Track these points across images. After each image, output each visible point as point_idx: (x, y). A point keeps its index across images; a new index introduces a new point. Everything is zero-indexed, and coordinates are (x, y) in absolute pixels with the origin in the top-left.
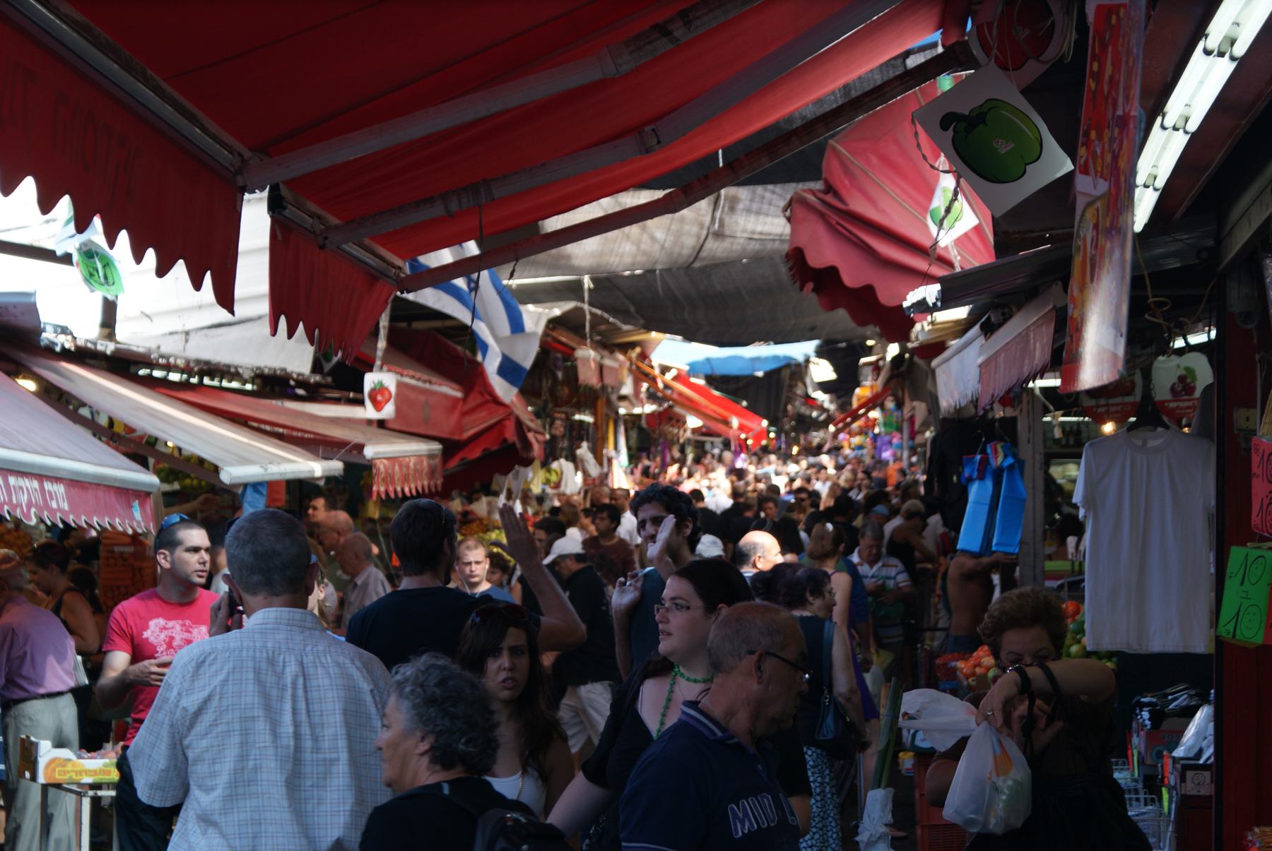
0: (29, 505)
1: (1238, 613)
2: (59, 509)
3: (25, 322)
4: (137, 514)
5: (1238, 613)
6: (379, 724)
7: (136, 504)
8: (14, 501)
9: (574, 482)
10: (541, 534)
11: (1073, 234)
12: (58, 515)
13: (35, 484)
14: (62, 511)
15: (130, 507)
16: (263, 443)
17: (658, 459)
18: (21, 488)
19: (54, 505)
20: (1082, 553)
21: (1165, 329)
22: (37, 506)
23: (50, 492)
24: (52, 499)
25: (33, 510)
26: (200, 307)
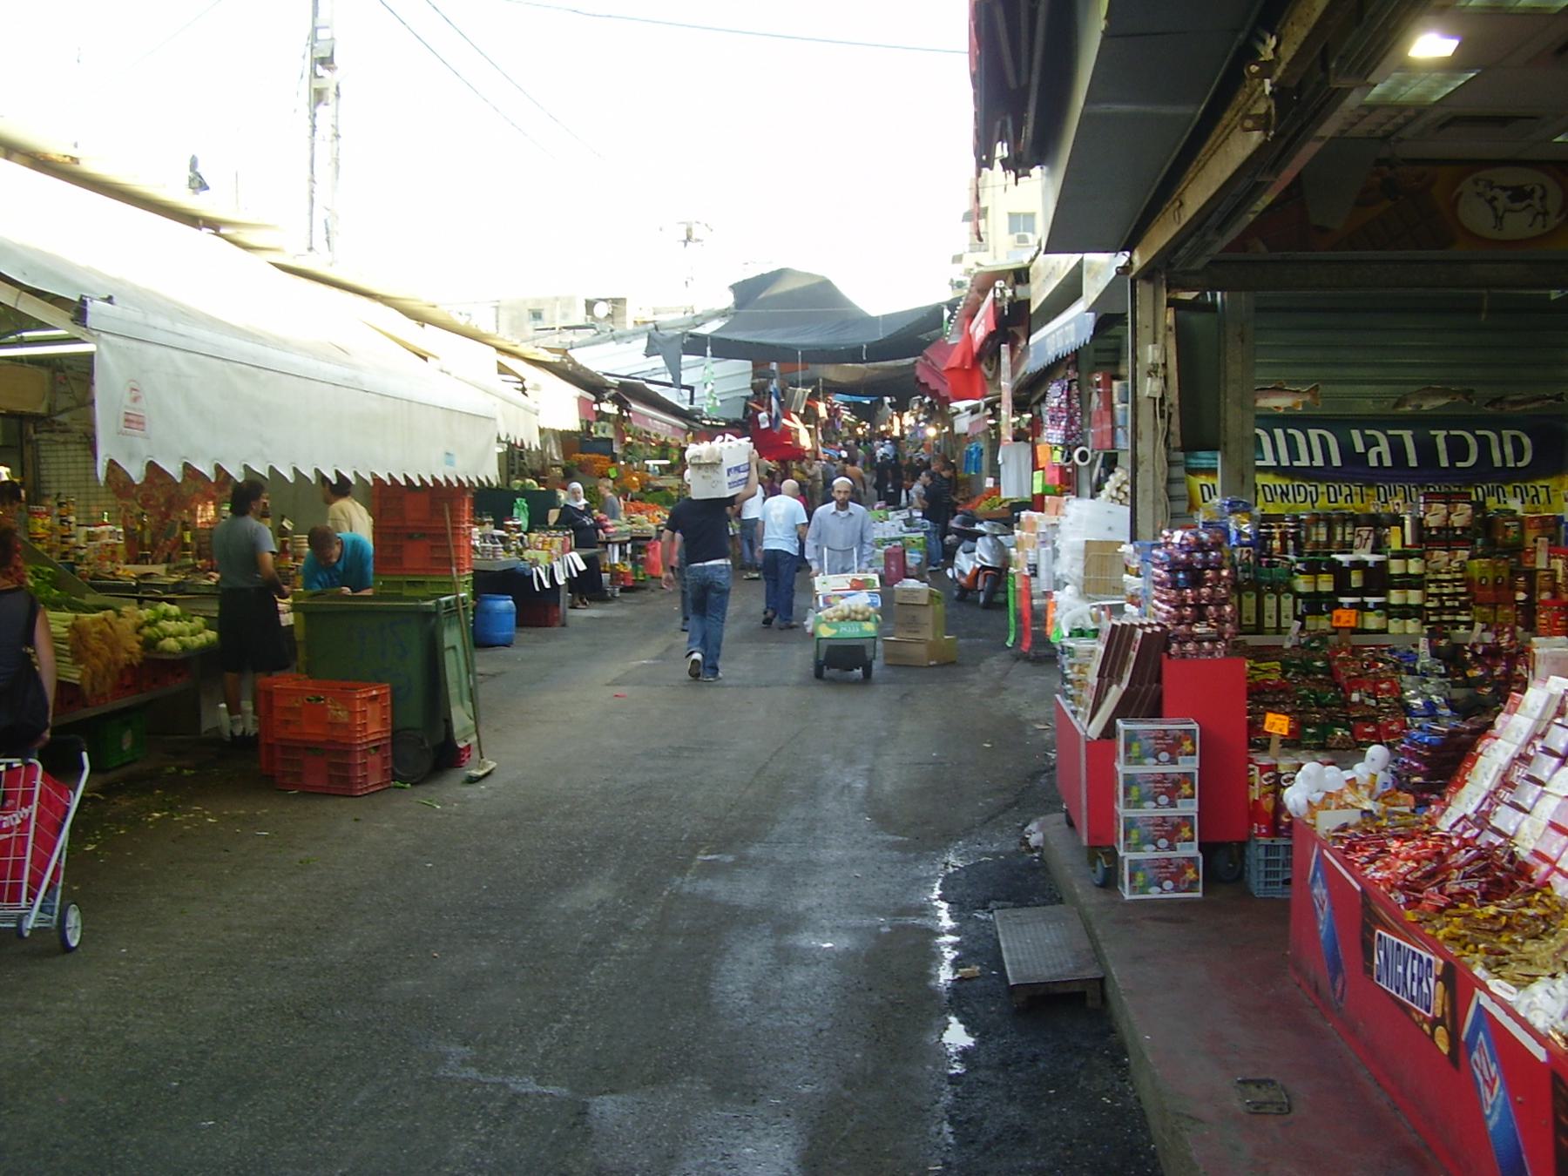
11: (808, 400)
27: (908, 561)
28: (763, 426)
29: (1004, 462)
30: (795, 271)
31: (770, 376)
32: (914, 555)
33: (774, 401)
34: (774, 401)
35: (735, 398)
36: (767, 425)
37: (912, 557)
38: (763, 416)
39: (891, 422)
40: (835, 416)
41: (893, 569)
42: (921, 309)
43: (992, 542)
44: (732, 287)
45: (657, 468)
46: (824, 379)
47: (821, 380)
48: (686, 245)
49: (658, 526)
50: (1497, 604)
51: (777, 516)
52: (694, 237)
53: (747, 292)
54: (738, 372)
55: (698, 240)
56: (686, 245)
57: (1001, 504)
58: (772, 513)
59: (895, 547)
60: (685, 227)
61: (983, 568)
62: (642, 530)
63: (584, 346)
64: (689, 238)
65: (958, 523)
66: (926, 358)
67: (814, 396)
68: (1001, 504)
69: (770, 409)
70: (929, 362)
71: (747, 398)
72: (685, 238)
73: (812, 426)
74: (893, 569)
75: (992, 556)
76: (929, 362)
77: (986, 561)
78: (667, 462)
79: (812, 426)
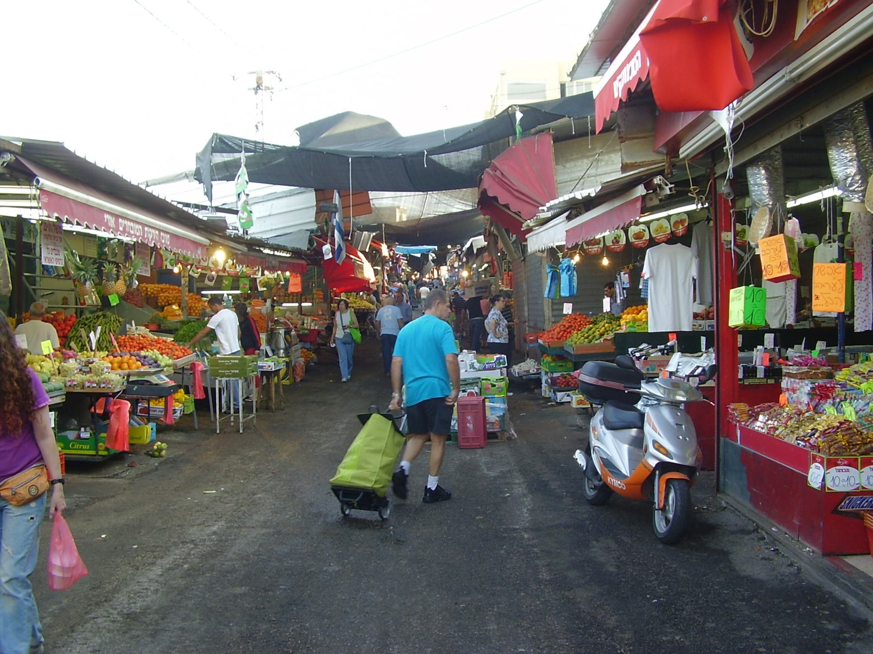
0: (152, 239)
1: (752, 314)
2: (165, 243)
3: (223, 224)
4: (199, 252)
5: (752, 314)
6: (849, 357)
7: (200, 248)
8: (146, 236)
9: (492, 627)
10: (771, 381)
11: (372, 241)
12: (164, 245)
13: (157, 232)
14: (166, 244)
15: (197, 249)
16: (177, 232)
17: (440, 529)
18: (150, 232)
19: (163, 241)
20: (378, 243)
21: (14, 556)
22: (155, 240)
23: (163, 237)
24: (163, 239)
25: (153, 242)
26: (272, 230)
27: (488, 413)
28: (326, 258)
29: (652, 276)
30: (354, 113)
31: (333, 211)
32: (498, 405)
33: (336, 234)
34: (336, 234)
35: (300, 231)
36: (330, 256)
37: (492, 408)
38: (327, 248)
39: (433, 273)
40: (397, 263)
41: (470, 426)
42: (476, 124)
43: (674, 416)
44: (297, 129)
45: (230, 297)
46: (385, 224)
47: (383, 225)
48: (256, 93)
49: (129, 376)
50: (180, 262)
51: (387, 316)
52: (264, 85)
53: (307, 132)
54: (303, 206)
55: (267, 88)
56: (256, 93)
57: (602, 335)
58: (385, 315)
59: (471, 394)
60: (255, 76)
61: (663, 467)
62: (98, 384)
63: (159, 183)
64: (259, 87)
65: (591, 375)
66: (495, 169)
67: (377, 240)
68: (602, 335)
69: (332, 243)
70: (498, 173)
71: (312, 231)
72: (255, 85)
73: (379, 268)
74: (470, 426)
75: (674, 440)
76: (498, 173)
77: (667, 453)
78: (238, 292)
79: (379, 268)
